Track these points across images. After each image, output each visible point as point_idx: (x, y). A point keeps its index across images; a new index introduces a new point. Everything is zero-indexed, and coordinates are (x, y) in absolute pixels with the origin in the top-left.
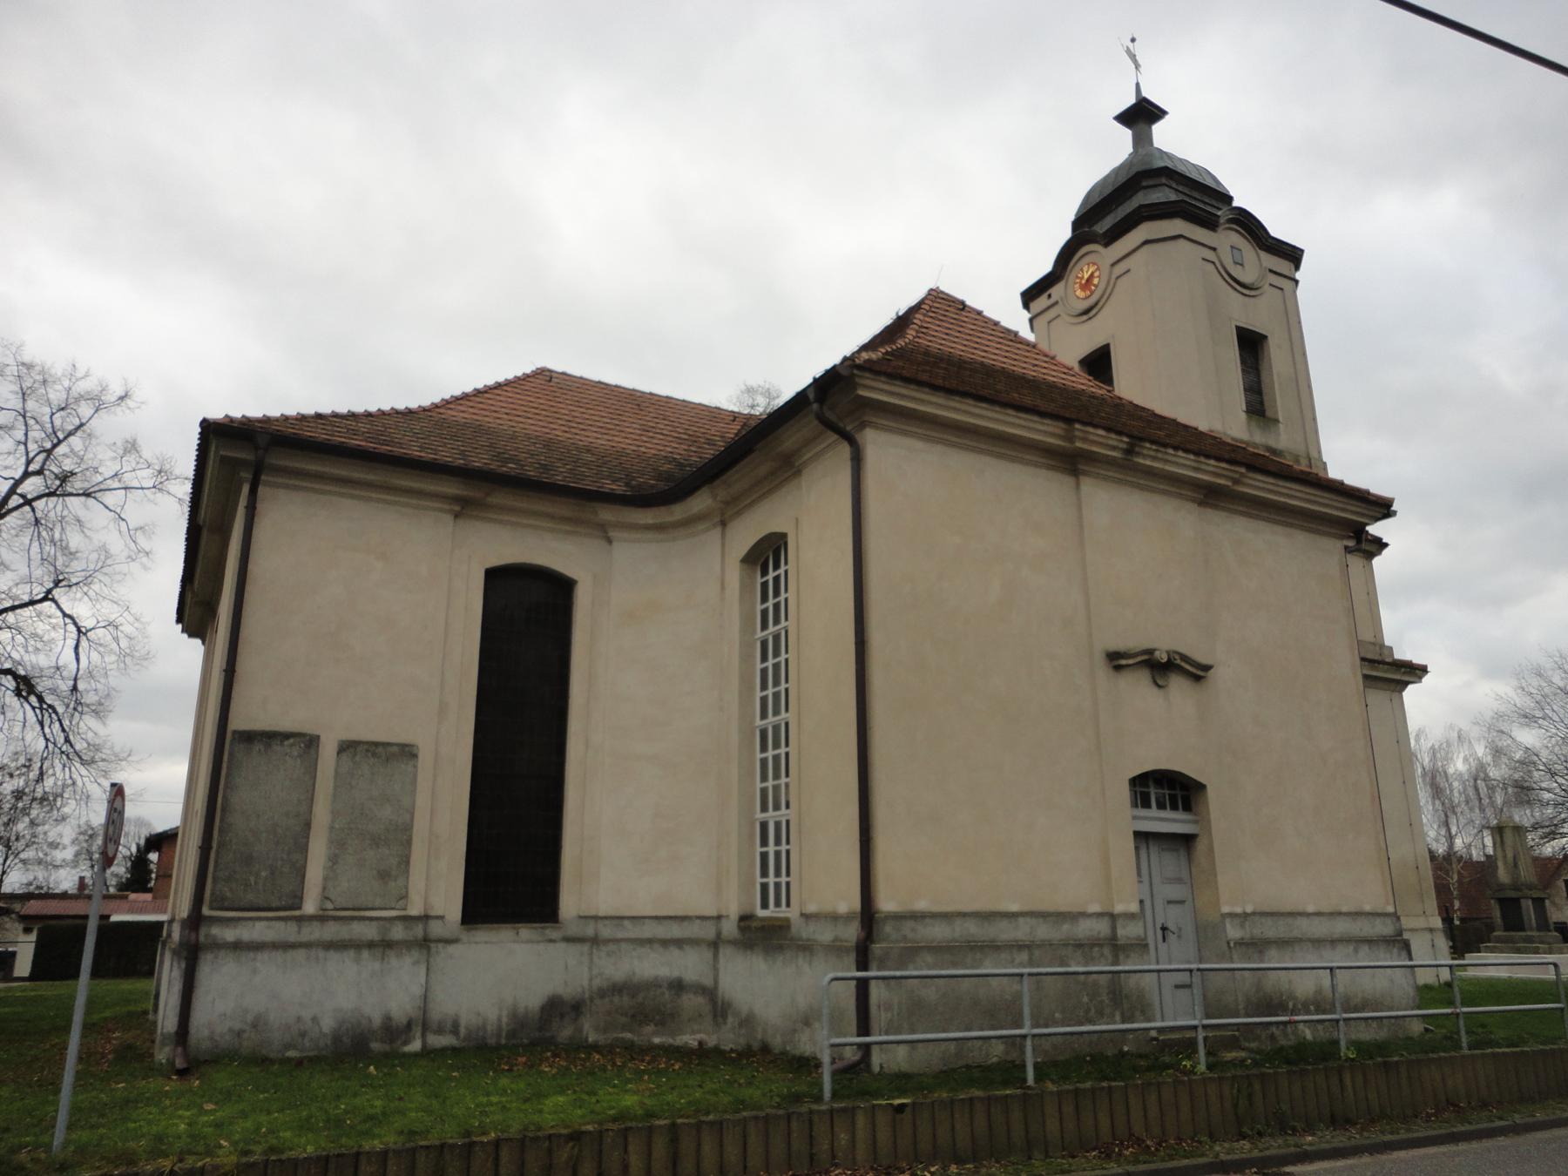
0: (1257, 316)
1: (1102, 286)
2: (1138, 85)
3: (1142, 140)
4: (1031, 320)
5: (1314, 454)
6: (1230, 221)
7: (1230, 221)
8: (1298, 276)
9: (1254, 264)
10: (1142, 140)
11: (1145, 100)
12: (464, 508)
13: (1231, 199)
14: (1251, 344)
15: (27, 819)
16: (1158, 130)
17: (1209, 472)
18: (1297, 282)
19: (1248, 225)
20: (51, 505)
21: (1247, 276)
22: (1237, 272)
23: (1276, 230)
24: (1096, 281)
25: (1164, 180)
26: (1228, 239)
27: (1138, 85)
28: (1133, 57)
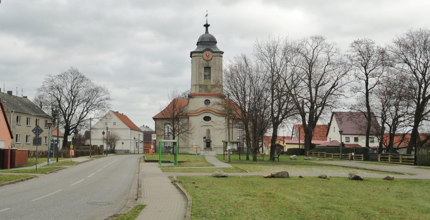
3: (207, 30)
10: (207, 30)
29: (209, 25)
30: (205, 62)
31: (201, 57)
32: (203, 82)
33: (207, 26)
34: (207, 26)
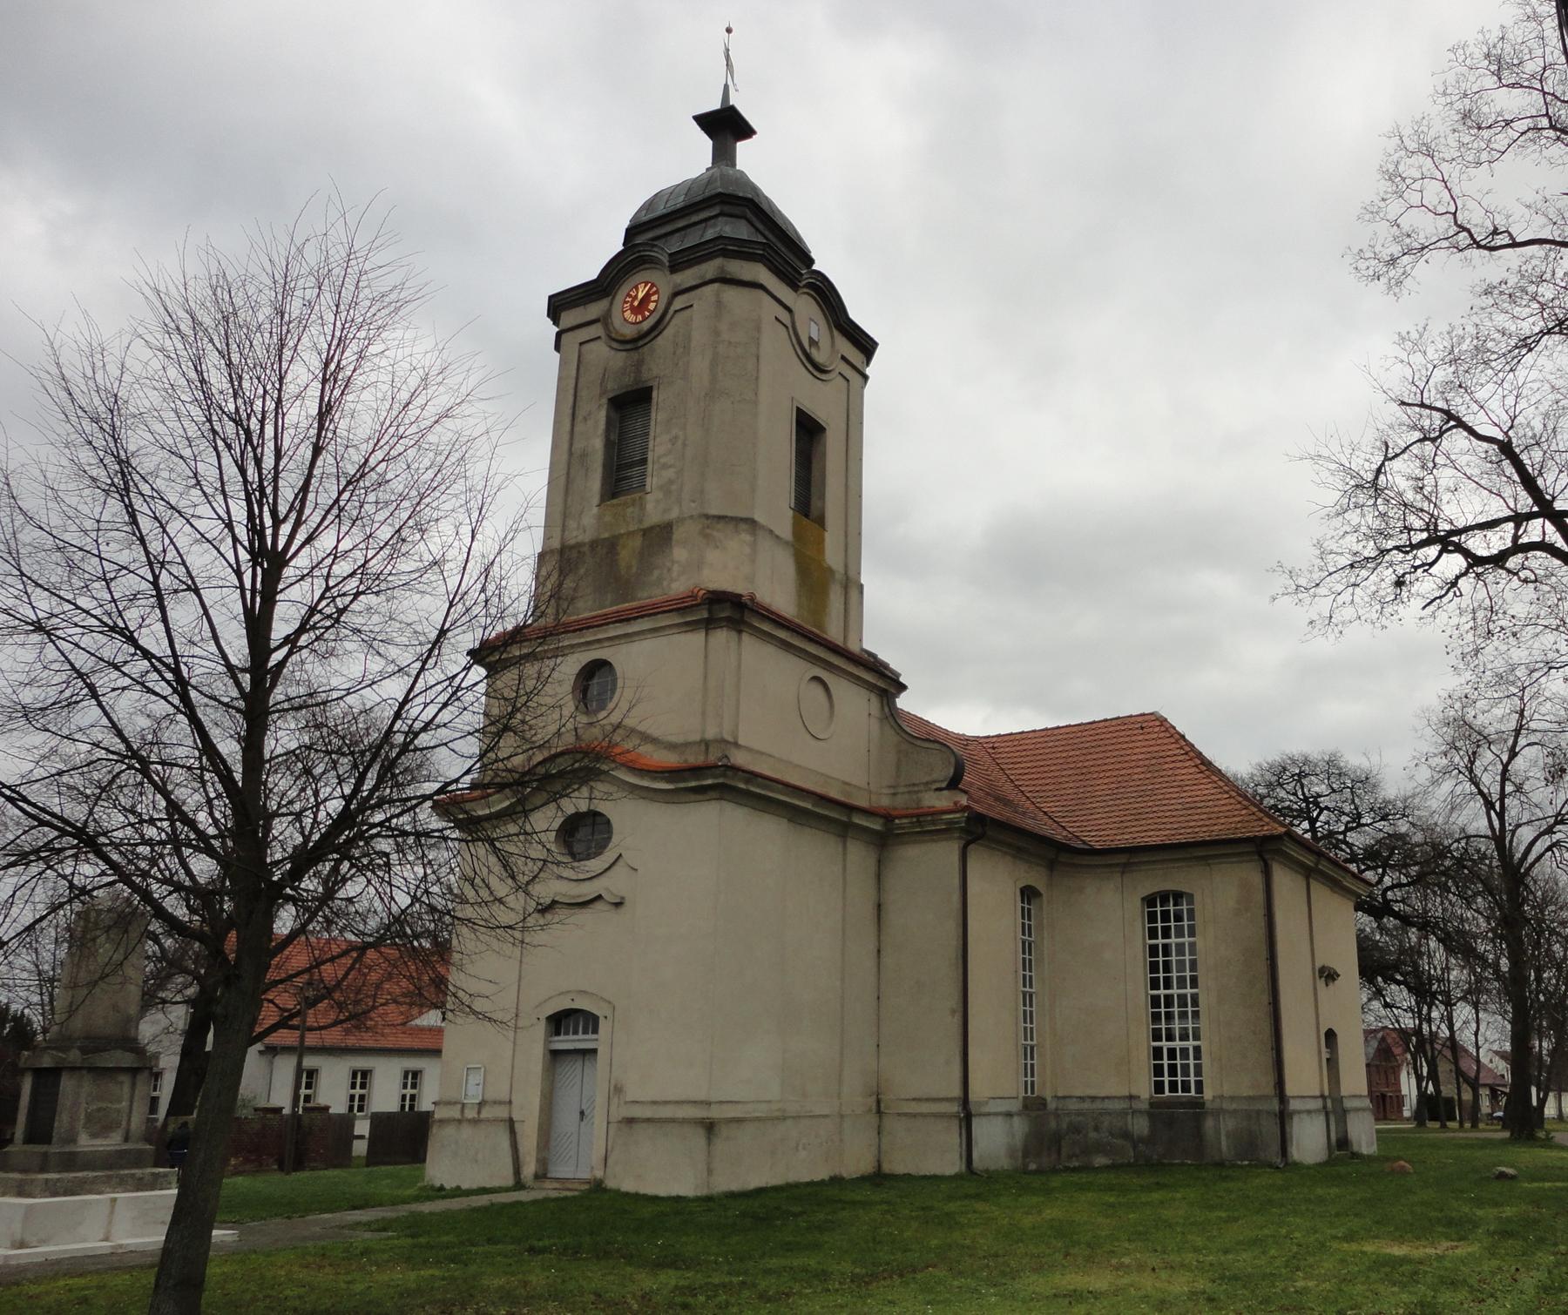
0: (822, 402)
1: (656, 316)
2: (726, 87)
3: (724, 154)
4: (559, 335)
5: (852, 574)
6: (809, 285)
7: (809, 285)
8: (868, 371)
9: (832, 347)
10: (724, 154)
11: (733, 109)
12: (1125, 868)
13: (812, 261)
14: (808, 430)
15: (26, 1011)
16: (743, 148)
17: (1122, 859)
18: (866, 378)
19: (826, 295)
20: (56, 666)
21: (820, 356)
22: (814, 353)
23: (858, 313)
24: (652, 306)
25: (749, 215)
26: (805, 307)
27: (726, 87)
28: (729, 65)
29: (745, 131)
30: (618, 359)
31: (596, 330)
32: (589, 522)
33: (725, 126)
34: (725, 126)
